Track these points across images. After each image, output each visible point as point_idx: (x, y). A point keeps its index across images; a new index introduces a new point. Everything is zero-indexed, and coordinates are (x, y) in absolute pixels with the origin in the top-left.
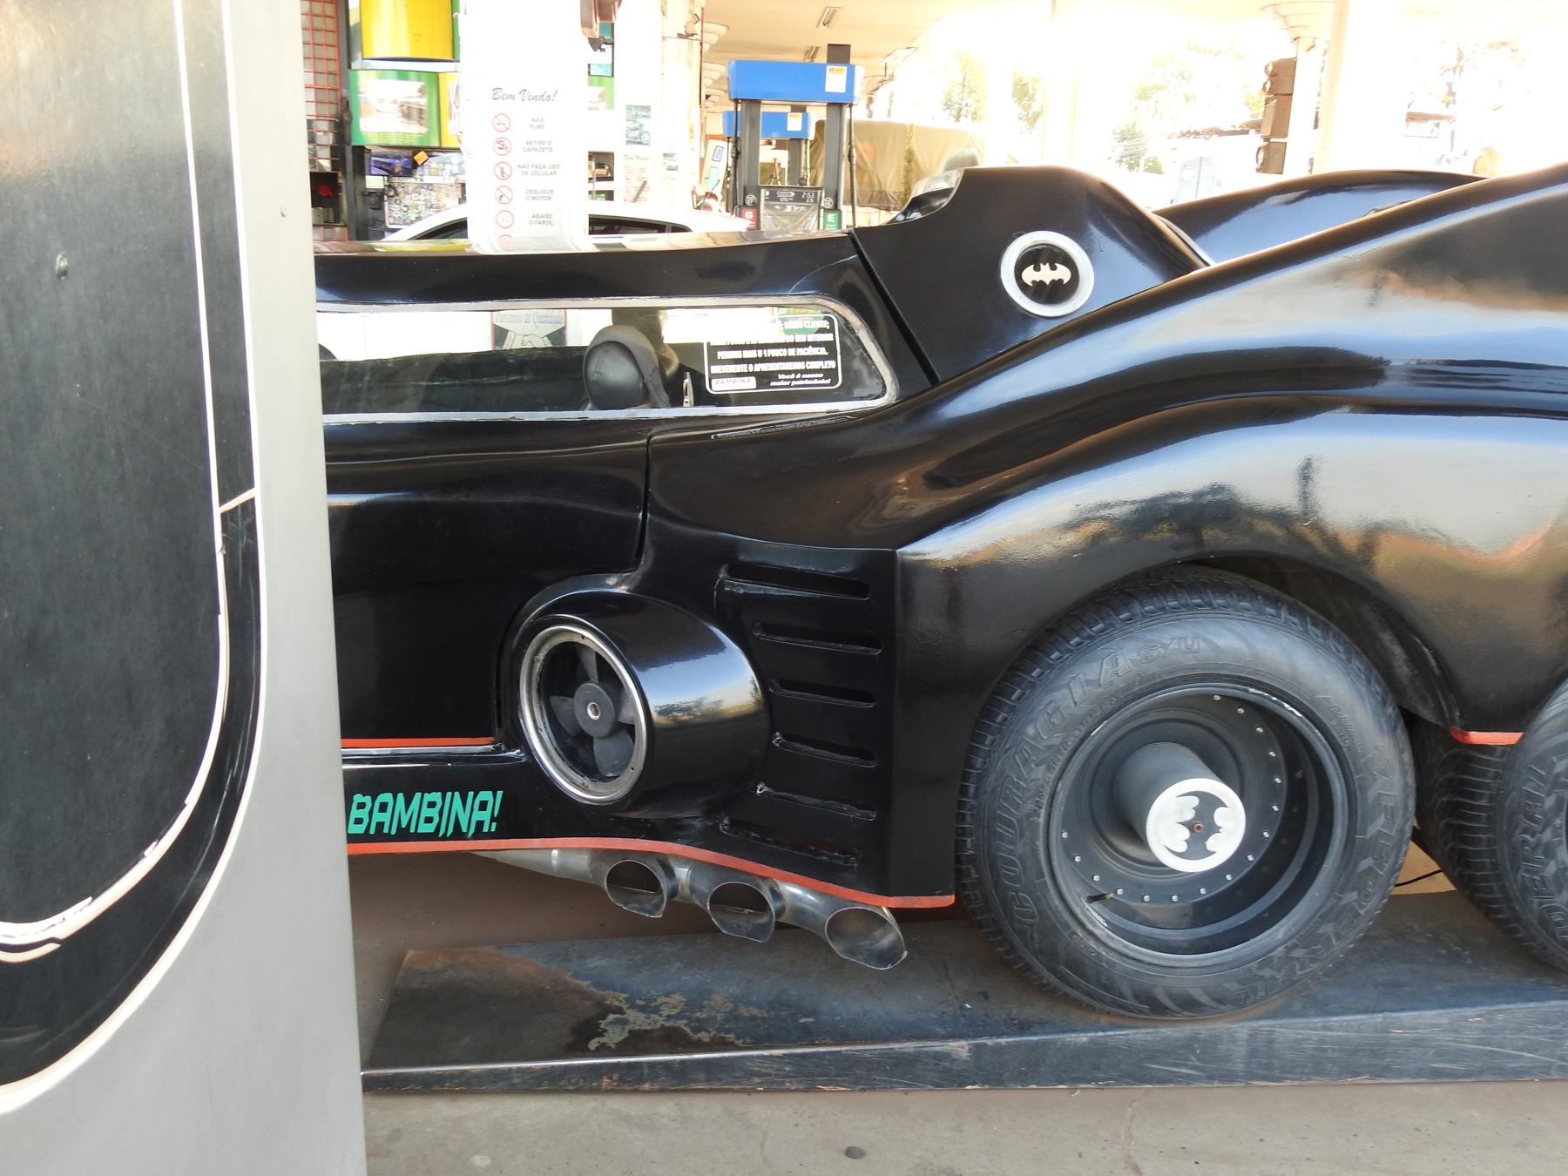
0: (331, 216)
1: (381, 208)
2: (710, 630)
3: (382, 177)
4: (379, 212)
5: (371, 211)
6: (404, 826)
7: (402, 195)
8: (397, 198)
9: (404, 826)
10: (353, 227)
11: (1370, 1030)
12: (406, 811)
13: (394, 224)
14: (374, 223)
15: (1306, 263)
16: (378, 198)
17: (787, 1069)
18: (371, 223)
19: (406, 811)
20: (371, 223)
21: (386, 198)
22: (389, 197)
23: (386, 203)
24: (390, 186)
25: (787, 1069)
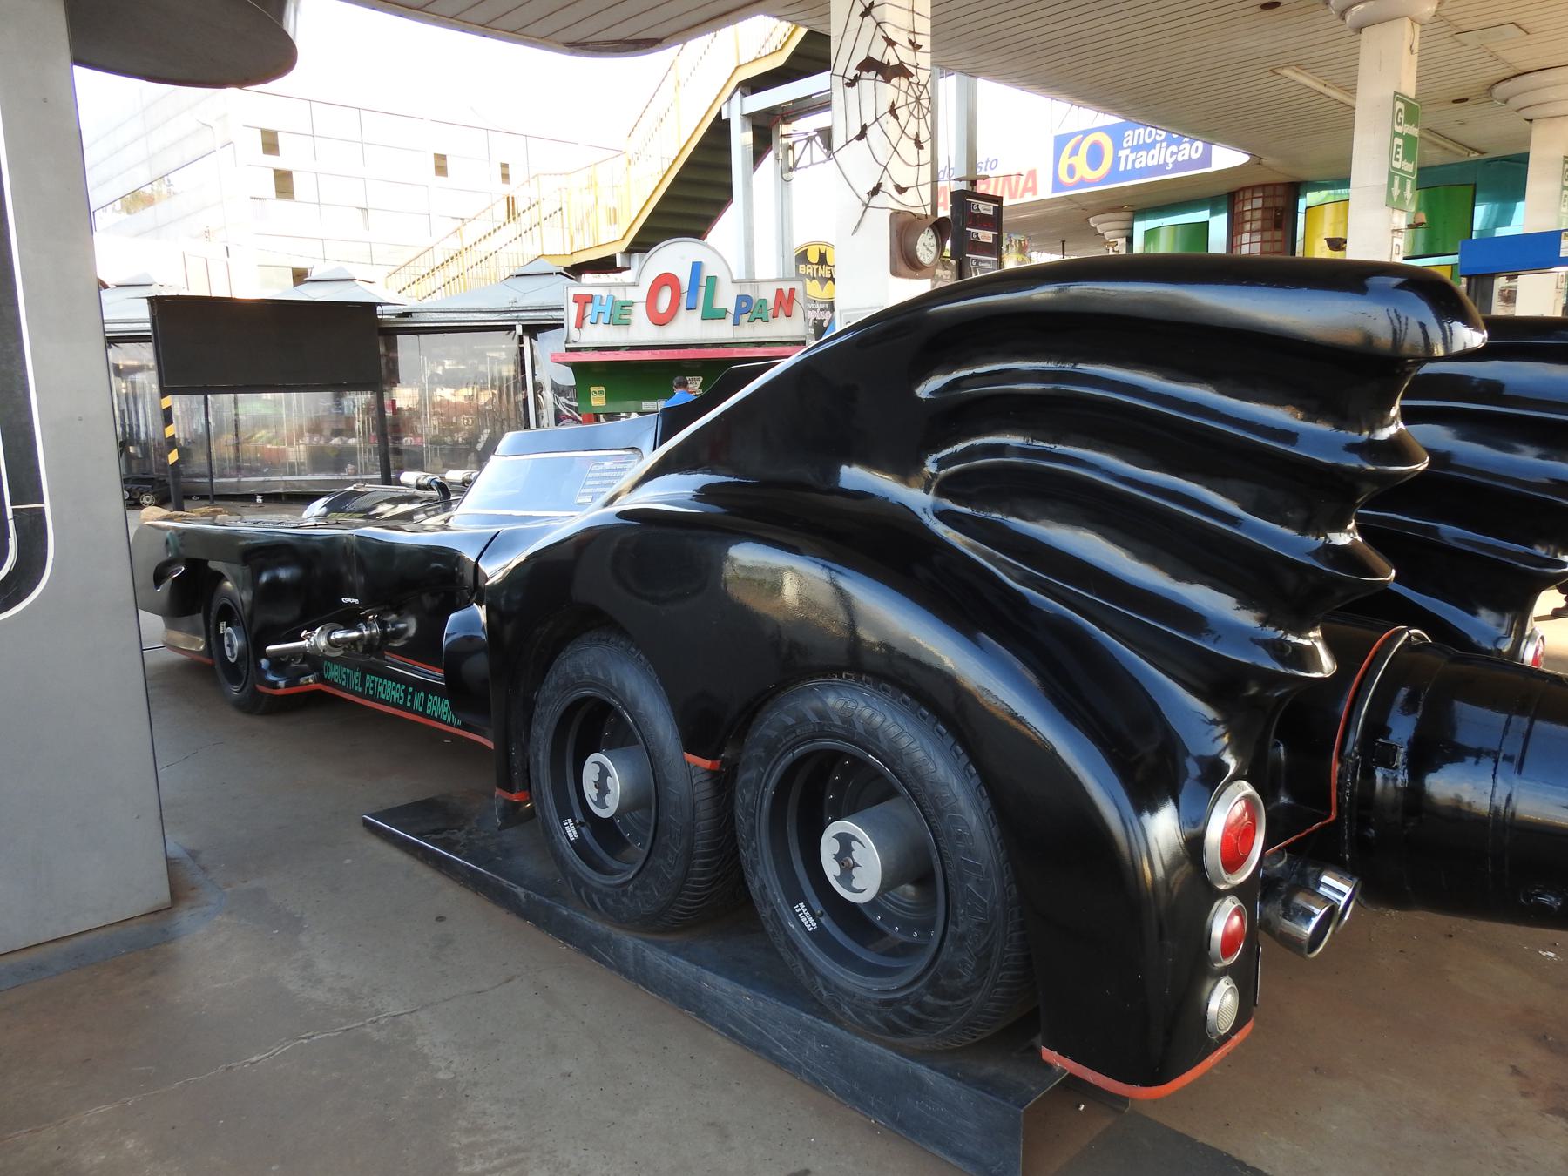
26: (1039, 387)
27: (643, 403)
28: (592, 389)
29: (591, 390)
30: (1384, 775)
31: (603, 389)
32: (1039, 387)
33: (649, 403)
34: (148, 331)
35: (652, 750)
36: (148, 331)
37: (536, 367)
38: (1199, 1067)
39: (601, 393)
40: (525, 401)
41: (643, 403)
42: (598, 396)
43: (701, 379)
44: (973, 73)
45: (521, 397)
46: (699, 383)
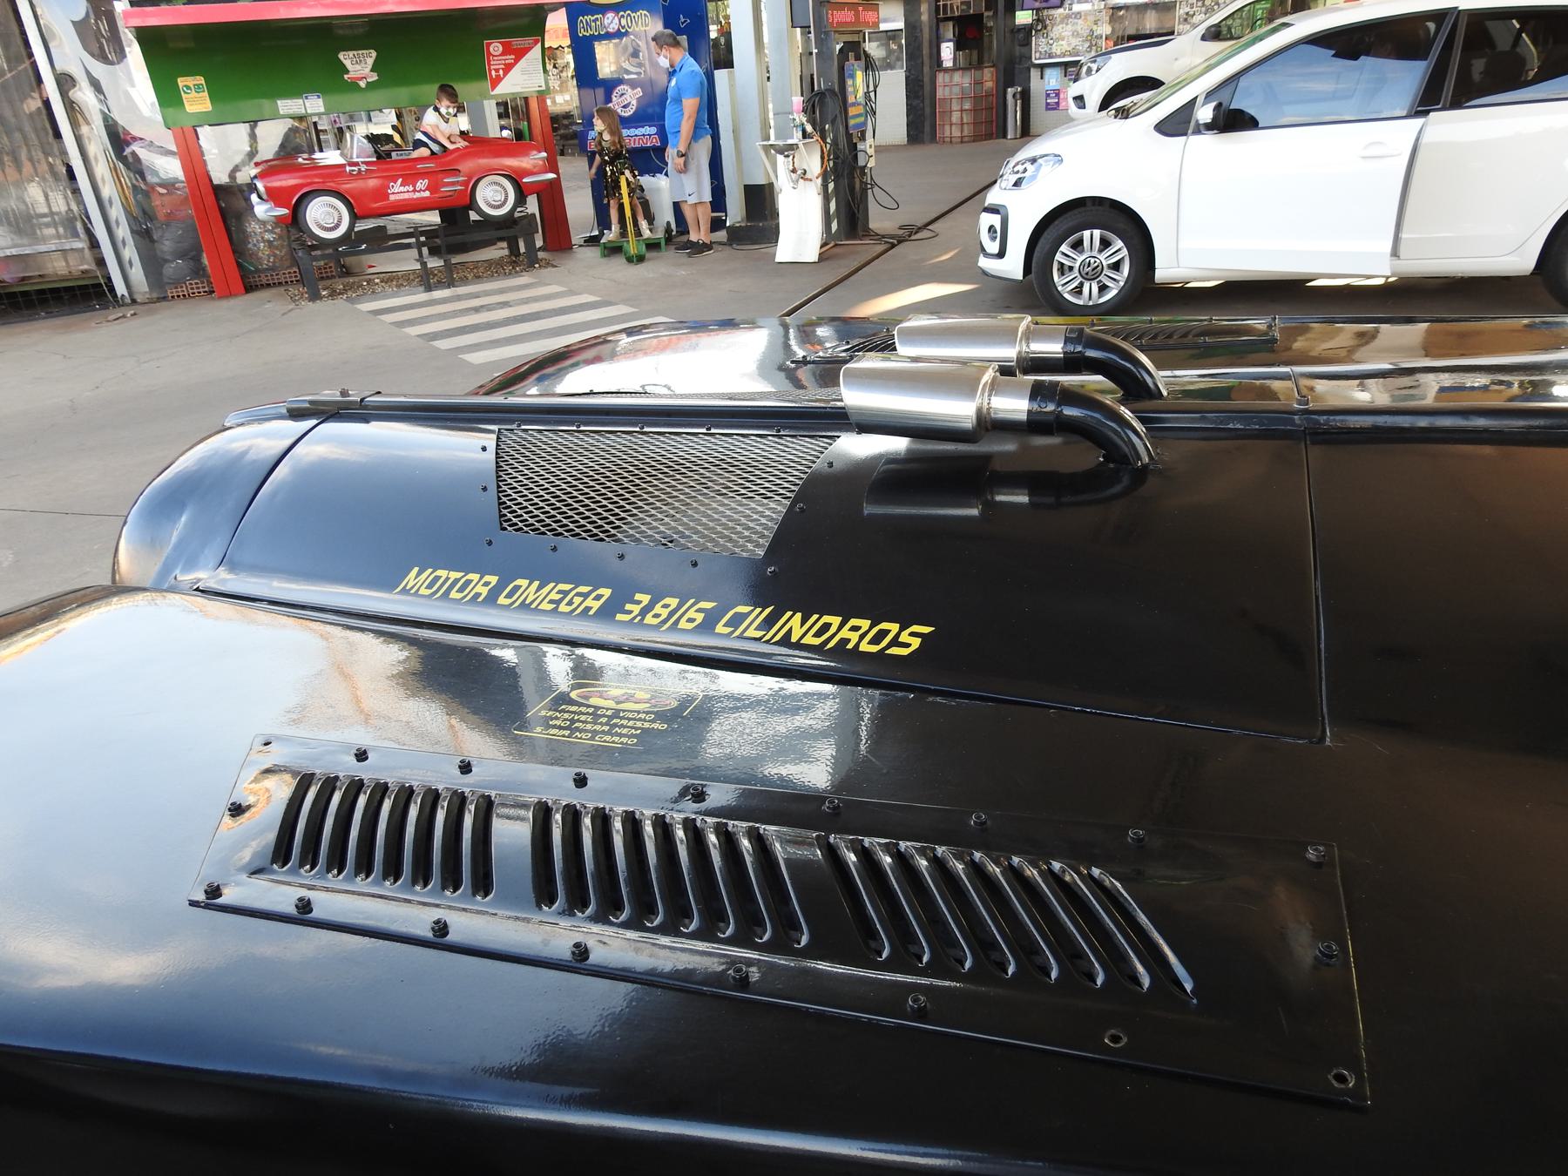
0: (975, 57)
1: (1029, 44)
2: (581, 1085)
3: (1031, 11)
4: (1026, 48)
5: (1017, 48)
6: (527, 602)
7: (1049, 28)
8: (1045, 31)
9: (527, 602)
10: (1001, 67)
11: (48, 184)
12: (535, 593)
13: (1040, 59)
14: (1020, 61)
15: (836, 1139)
16: (1027, 30)
17: (96, 547)
18: (1018, 60)
19: (535, 593)
20: (1018, 60)
21: (1034, 32)
22: (1037, 31)
23: (1034, 38)
24: (1038, 20)
25: (96, 547)
26: (480, 426)
27: (279, 102)
28: (181, 82)
29: (180, 85)
30: (1314, 391)
31: (201, 80)
32: (480, 426)
33: (289, 102)
34: (1059, 353)
35: (1111, 58)
36: (1059, 353)
37: (51, 45)
38: (773, 1144)
39: (198, 88)
40: (47, 104)
41: (279, 102)
42: (194, 94)
43: (374, 54)
44: (450, 571)
45: (34, 104)
46: (370, 61)
